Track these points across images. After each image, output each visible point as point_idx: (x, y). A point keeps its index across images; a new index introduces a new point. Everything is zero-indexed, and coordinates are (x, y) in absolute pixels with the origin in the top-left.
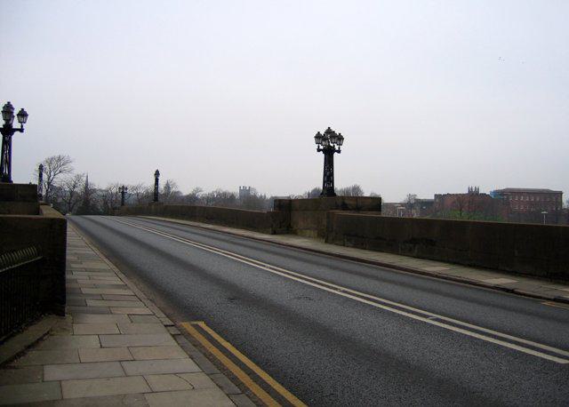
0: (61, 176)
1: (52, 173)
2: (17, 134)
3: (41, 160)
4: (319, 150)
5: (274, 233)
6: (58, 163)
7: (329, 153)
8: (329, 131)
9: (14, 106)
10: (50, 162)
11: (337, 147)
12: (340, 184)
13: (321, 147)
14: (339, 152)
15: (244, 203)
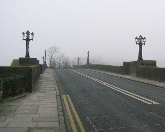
0: (55, 54)
1: (53, 53)
2: (31, 41)
3: (47, 48)
4: (137, 44)
5: (122, 74)
6: (54, 49)
7: (141, 44)
8: (140, 36)
9: (30, 32)
10: (51, 48)
11: (143, 43)
12: (145, 58)
13: (138, 43)
14: (144, 44)
15: (72, 61)
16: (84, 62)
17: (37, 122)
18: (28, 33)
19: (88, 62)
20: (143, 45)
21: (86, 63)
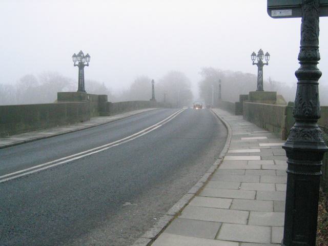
7: (81, 66)
11: (86, 63)
14: (88, 65)
16: (148, 99)
17: (248, 212)
18: (261, 53)
19: (153, 97)
20: (85, 68)
21: (151, 98)
